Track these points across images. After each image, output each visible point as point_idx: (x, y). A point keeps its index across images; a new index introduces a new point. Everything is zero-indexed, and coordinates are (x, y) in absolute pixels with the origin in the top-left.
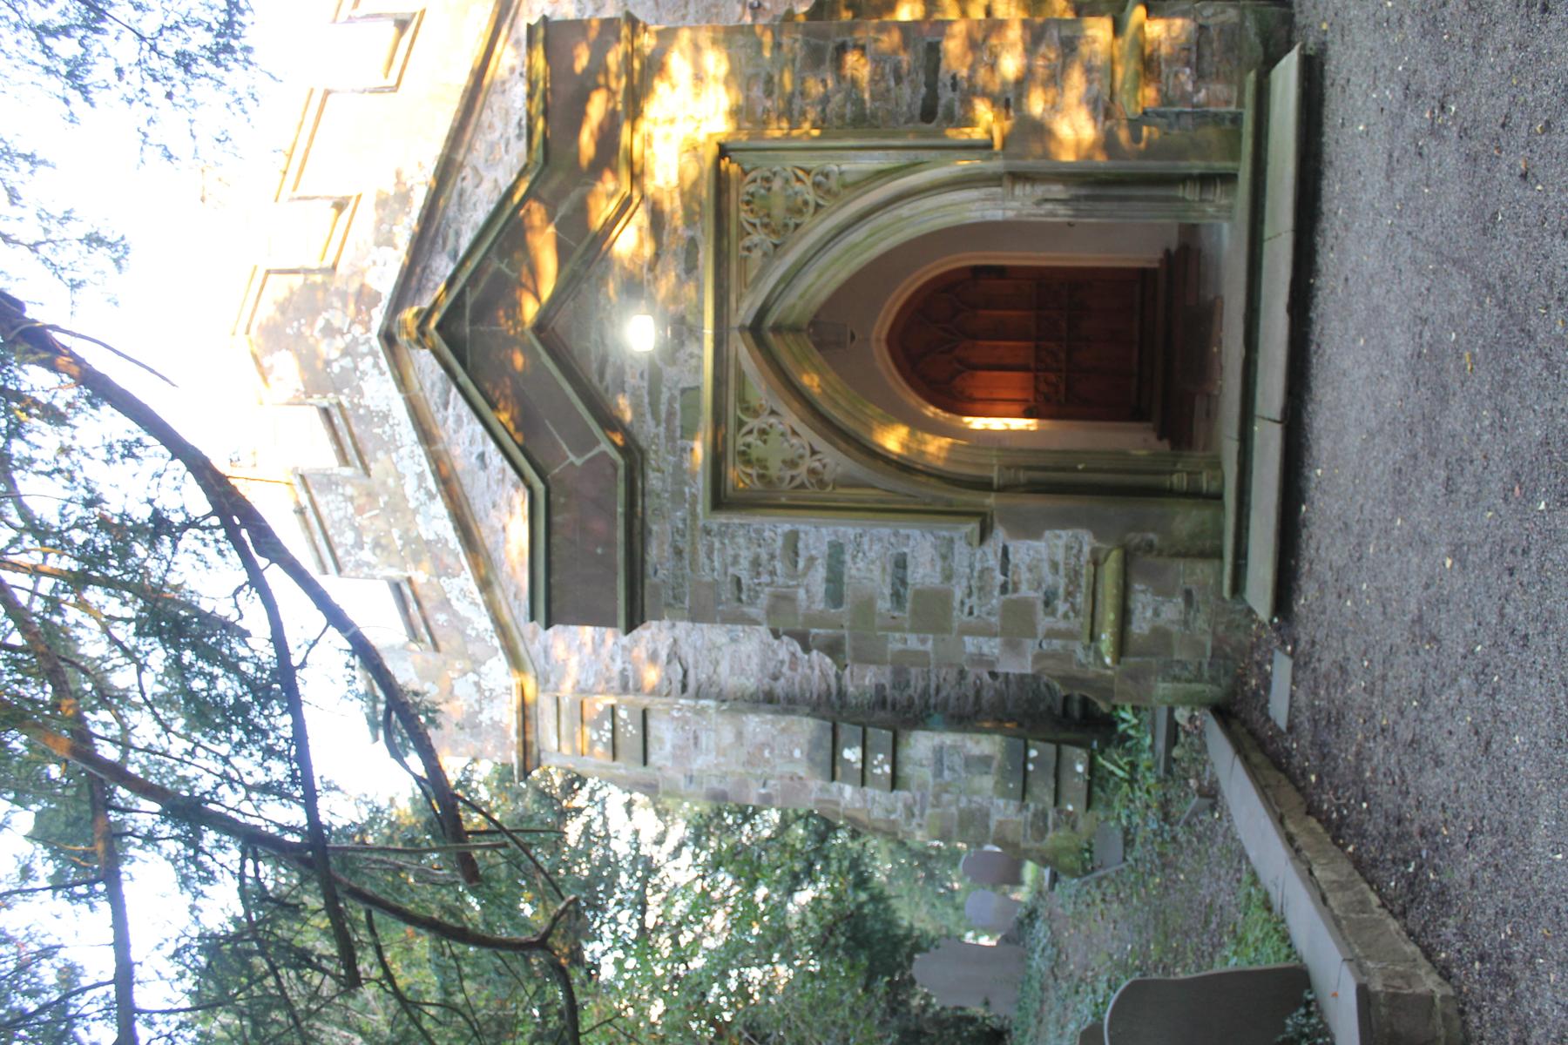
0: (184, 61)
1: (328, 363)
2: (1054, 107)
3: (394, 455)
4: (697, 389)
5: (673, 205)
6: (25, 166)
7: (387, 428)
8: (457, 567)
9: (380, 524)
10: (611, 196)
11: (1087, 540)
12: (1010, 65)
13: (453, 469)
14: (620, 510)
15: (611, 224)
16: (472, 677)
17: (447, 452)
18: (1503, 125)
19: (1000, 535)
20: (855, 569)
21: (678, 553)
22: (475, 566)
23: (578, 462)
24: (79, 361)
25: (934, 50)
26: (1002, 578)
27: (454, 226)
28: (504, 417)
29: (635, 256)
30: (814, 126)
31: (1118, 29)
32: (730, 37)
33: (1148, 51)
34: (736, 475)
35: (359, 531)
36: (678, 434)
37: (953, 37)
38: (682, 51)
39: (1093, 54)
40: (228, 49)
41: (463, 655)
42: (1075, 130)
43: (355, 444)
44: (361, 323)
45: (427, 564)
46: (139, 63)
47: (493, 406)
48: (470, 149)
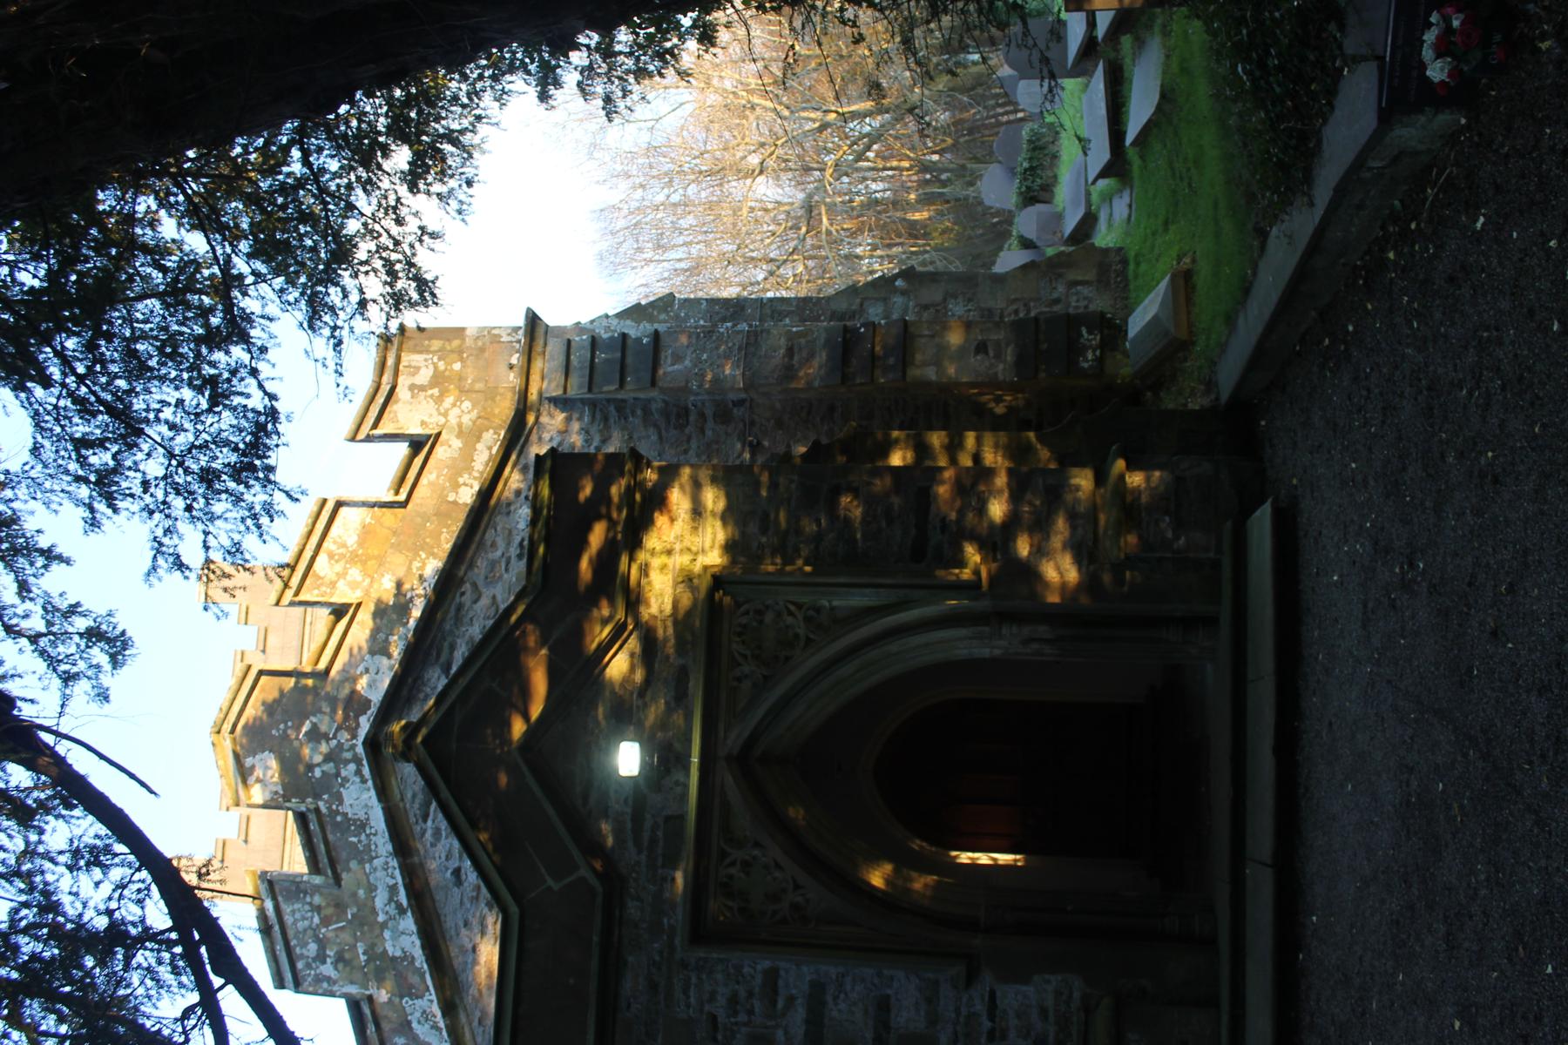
0: (208, 477)
1: (310, 767)
2: (1040, 551)
3: (367, 866)
4: (681, 818)
5: (665, 632)
6: (40, 562)
7: (363, 837)
8: (422, 987)
9: (346, 937)
10: (605, 622)
12: (997, 510)
13: (427, 884)
15: (604, 648)
17: (422, 865)
18: (1470, 584)
22: (439, 988)
23: (556, 886)
24: (61, 762)
25: (925, 497)
26: (989, 1024)
27: (449, 639)
28: (484, 837)
29: (626, 680)
30: (806, 564)
31: (1100, 479)
32: (727, 477)
33: (1129, 498)
35: (322, 944)
36: (660, 862)
37: (942, 482)
38: (682, 487)
39: (1077, 501)
40: (252, 468)
43: (328, 852)
44: (348, 729)
45: (389, 984)
46: (165, 477)
47: (474, 825)
48: (471, 566)
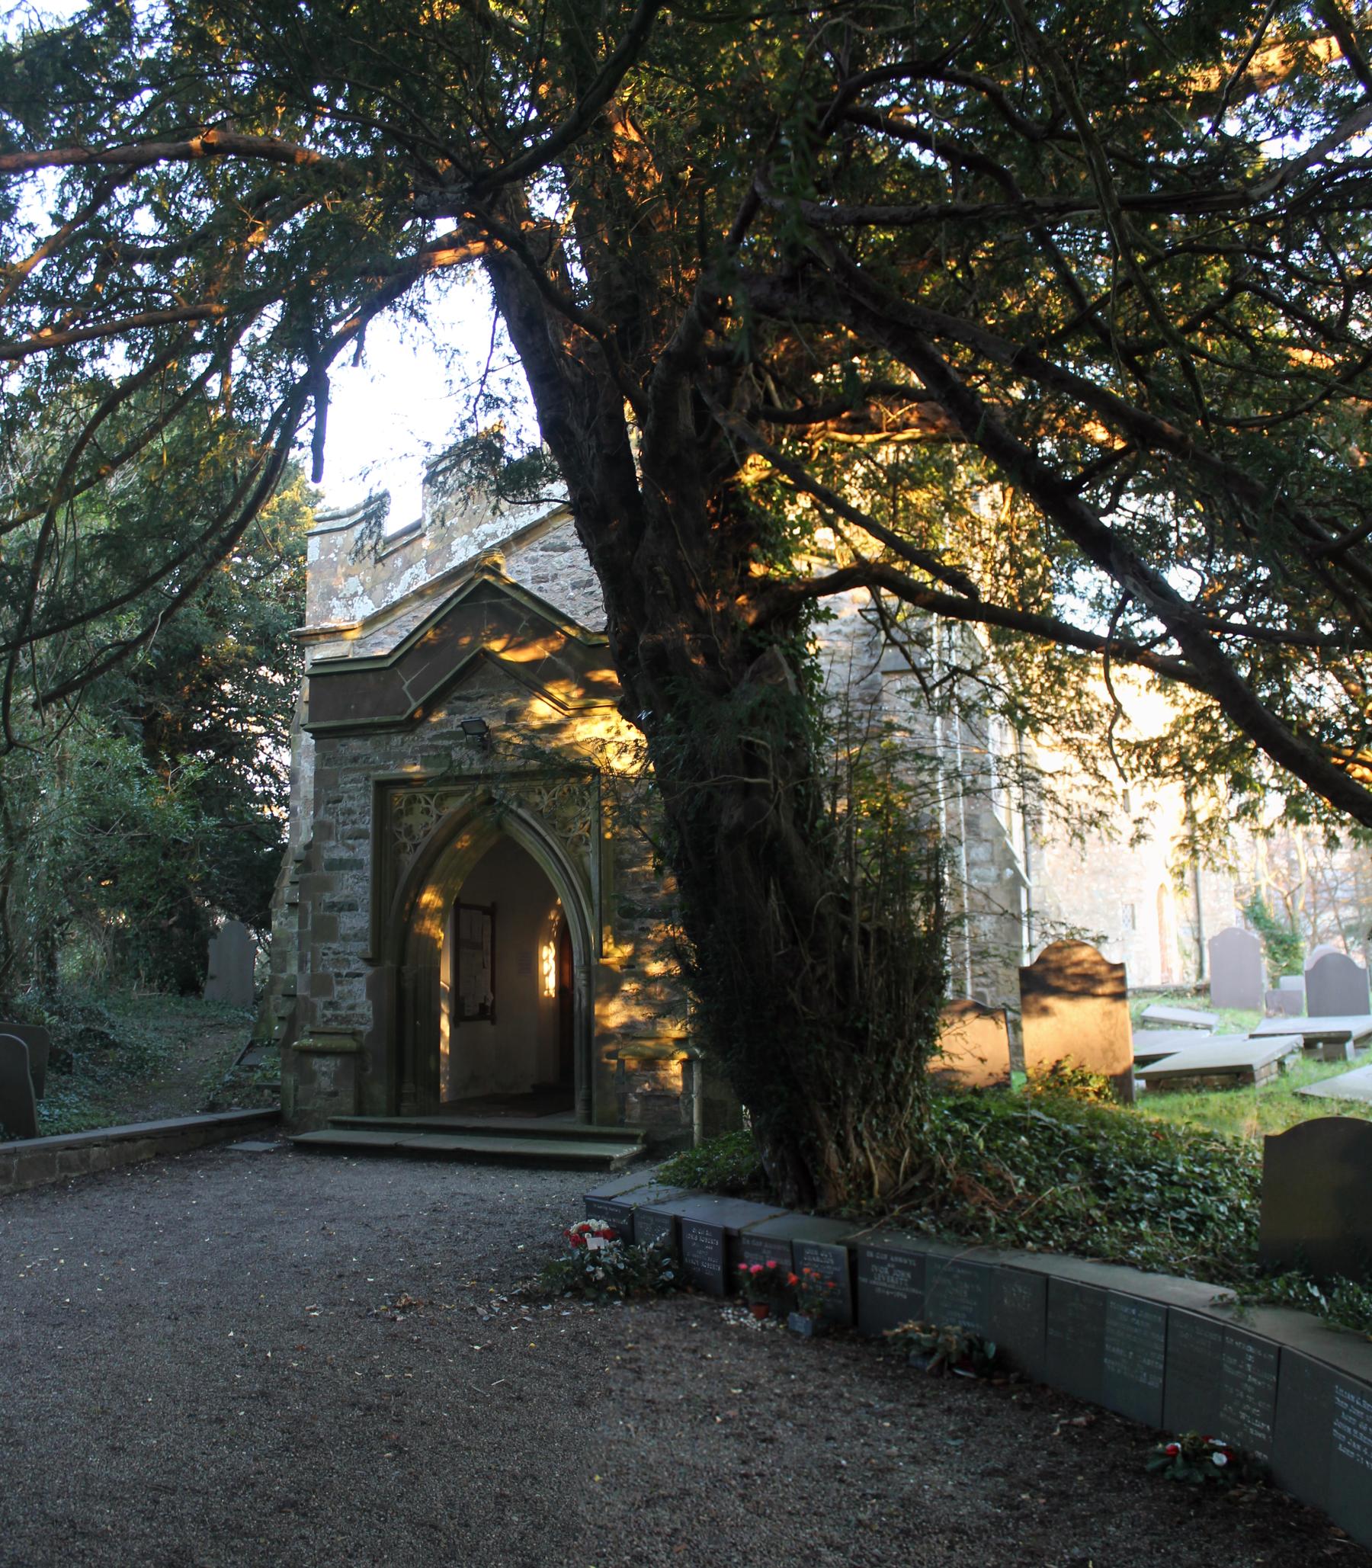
2: (627, 999)
5: (565, 738)
10: (567, 695)
11: (366, 1028)
14: (376, 719)
16: (360, 590)
19: (369, 971)
20: (348, 877)
21: (355, 760)
28: (430, 634)
29: (532, 715)
34: (402, 793)
41: (375, 582)
45: (433, 547)
47: (437, 626)
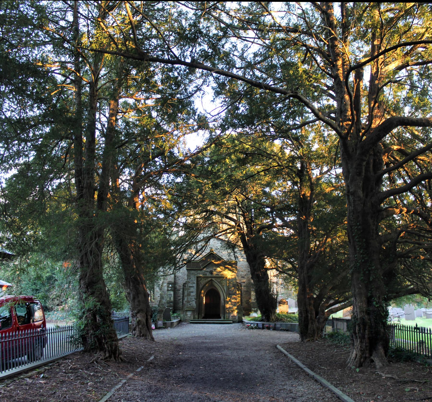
5: (222, 273)
12: (233, 301)
25: (234, 294)
42: (228, 306)
